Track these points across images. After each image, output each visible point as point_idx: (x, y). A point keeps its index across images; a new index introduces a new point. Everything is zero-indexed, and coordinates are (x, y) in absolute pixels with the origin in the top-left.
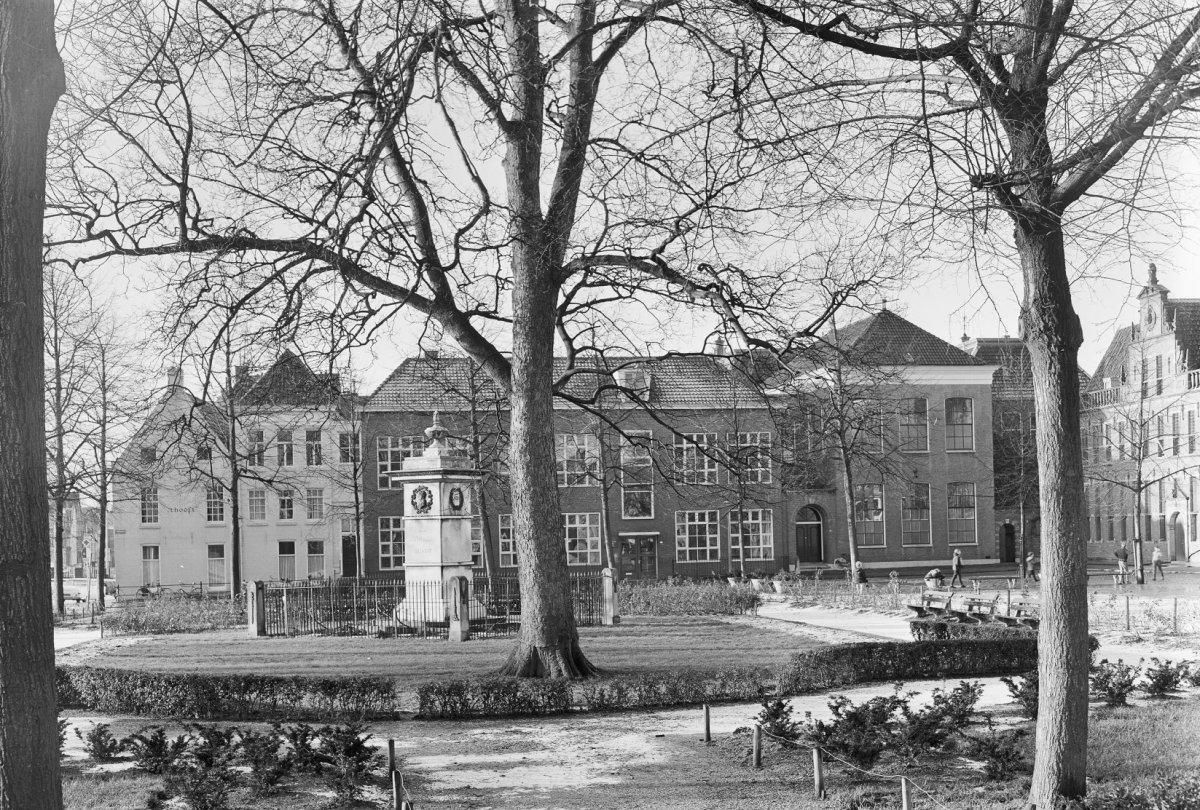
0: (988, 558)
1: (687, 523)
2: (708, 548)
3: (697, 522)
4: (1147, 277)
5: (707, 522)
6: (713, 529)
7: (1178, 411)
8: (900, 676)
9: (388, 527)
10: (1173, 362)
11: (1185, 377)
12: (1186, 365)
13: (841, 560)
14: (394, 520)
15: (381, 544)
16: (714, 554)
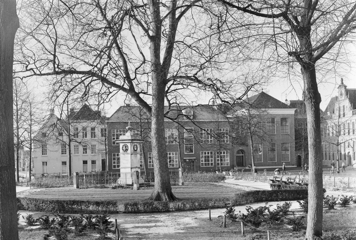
0: (293, 165)
1: (204, 155)
2: (210, 162)
3: (207, 155)
4: (340, 82)
5: (210, 155)
6: (212, 157)
7: (350, 122)
8: (267, 200)
9: (115, 156)
10: (348, 107)
11: (352, 112)
12: (352, 108)
13: (249, 166)
14: (117, 154)
15: (113, 161)
16: (212, 164)
